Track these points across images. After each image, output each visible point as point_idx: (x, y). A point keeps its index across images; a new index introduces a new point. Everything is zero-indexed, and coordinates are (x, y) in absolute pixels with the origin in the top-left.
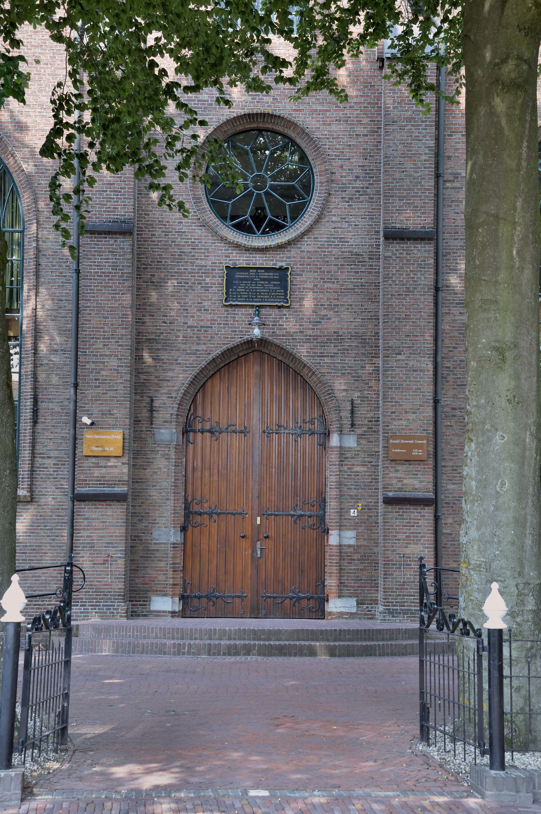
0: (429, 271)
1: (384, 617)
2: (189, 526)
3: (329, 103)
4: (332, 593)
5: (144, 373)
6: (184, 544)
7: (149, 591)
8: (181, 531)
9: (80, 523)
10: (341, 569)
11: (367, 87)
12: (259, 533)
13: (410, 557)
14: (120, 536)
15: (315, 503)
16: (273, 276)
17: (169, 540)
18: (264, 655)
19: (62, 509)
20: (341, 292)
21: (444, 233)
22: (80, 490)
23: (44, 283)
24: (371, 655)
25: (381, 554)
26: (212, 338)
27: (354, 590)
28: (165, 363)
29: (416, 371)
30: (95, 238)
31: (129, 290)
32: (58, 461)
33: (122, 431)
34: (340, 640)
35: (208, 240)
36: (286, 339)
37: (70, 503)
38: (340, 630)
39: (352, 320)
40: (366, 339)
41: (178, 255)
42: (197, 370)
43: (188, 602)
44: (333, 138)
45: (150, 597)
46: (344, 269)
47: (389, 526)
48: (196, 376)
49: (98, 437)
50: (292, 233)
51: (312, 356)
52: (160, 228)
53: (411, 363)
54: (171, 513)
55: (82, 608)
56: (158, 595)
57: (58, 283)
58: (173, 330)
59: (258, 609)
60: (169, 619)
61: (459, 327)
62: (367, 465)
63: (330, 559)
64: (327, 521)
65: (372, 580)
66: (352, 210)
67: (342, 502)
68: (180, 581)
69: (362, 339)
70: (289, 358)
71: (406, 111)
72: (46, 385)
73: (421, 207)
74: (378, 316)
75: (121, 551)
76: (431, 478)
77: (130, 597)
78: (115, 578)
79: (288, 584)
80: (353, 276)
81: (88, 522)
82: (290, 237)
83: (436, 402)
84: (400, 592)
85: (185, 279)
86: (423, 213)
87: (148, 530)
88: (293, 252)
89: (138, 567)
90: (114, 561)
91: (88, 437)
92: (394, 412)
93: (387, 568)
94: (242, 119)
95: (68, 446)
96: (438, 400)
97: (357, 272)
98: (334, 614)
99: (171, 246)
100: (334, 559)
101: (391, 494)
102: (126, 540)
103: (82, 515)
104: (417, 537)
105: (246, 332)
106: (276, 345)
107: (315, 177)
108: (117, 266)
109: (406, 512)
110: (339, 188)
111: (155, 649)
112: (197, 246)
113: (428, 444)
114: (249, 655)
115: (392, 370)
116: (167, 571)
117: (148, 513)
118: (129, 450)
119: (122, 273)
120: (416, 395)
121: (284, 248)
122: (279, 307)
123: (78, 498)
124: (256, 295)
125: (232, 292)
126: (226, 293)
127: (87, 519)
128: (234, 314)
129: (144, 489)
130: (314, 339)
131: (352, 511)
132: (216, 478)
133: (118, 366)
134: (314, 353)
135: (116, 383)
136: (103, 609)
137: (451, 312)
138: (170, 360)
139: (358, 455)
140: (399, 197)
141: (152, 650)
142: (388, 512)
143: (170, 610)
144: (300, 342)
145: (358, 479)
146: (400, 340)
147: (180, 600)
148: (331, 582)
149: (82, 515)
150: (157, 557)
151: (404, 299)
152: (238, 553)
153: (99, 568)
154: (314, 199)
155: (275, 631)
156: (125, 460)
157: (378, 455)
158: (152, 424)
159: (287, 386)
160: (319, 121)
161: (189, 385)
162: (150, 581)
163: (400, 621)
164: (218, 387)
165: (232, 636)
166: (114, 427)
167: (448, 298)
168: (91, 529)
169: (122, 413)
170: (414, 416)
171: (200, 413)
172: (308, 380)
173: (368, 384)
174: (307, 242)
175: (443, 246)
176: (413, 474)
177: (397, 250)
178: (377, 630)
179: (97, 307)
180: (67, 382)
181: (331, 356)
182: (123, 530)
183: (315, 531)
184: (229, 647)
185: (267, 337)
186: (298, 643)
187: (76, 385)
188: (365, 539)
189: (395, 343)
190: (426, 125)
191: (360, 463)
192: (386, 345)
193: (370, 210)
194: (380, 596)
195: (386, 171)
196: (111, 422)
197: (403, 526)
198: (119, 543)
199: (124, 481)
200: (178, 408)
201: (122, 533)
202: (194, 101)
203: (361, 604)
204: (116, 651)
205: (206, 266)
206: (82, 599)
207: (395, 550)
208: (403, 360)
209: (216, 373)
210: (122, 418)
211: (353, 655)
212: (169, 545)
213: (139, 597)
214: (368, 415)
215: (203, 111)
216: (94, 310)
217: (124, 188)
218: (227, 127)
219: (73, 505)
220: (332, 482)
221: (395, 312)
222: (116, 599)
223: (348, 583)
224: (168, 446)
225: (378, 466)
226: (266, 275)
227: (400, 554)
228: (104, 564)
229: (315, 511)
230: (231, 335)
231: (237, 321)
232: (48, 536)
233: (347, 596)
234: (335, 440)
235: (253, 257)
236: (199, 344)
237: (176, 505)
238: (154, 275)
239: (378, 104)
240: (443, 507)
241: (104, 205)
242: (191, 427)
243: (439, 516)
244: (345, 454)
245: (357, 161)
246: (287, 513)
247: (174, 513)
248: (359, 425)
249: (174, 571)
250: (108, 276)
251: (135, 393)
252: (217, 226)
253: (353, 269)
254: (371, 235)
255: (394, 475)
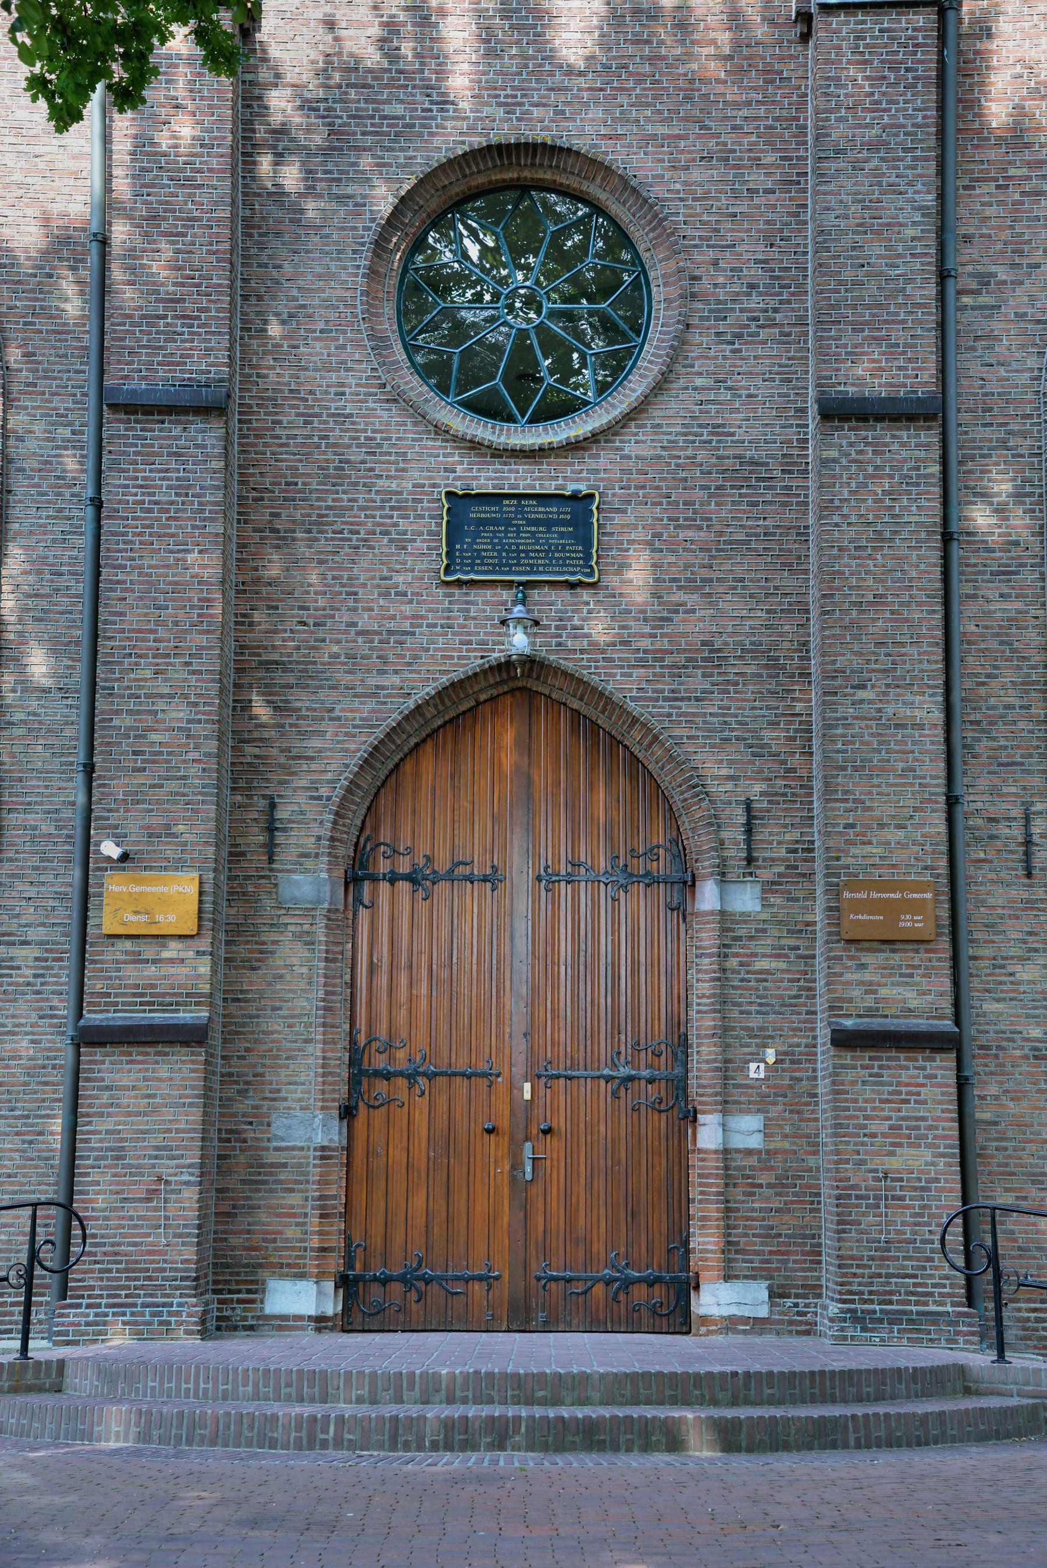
0: (927, 493)
1: (842, 1329)
2: (361, 1104)
3: (686, 119)
4: (709, 1268)
5: (255, 740)
6: (349, 1149)
7: (260, 1266)
8: (341, 1118)
9: (93, 1098)
10: (728, 1210)
11: (772, 81)
12: (528, 1121)
13: (901, 1180)
14: (188, 1131)
15: (663, 1047)
16: (558, 513)
17: (310, 1139)
18: (545, 1448)
19: (54, 1067)
20: (718, 550)
21: (959, 411)
22: (93, 1018)
23: (18, 533)
24: (834, 1446)
25: (828, 1171)
26: (415, 657)
27: (762, 1262)
28: (305, 718)
29: (903, 726)
30: (137, 421)
31: (216, 543)
32: (47, 951)
33: (196, 875)
34: (747, 1402)
35: (404, 432)
36: (589, 660)
37: (70, 1051)
38: (748, 1375)
39: (744, 613)
40: (777, 659)
41: (336, 468)
42: (380, 733)
43: (357, 1292)
44: (694, 199)
45: (264, 1282)
46: (723, 495)
47: (846, 1100)
48: (376, 748)
49: (137, 889)
50: (600, 416)
51: (651, 699)
52: (292, 407)
53: (890, 710)
54: (316, 1075)
55: (92, 1311)
56: (283, 1276)
57: (53, 532)
58: (324, 640)
59: (527, 1309)
60: (308, 1337)
61: (1001, 627)
62: (786, 956)
63: (701, 1185)
64: (692, 1091)
65: (805, 1236)
66: (739, 362)
67: (728, 1045)
68: (337, 1241)
69: (769, 658)
70: (597, 704)
71: (867, 126)
72: (20, 771)
73: (906, 345)
74: (807, 604)
75: (190, 1166)
76: (947, 984)
77: (215, 1282)
78: (175, 1236)
79: (599, 1247)
80: (744, 511)
81: (111, 1097)
82: (597, 425)
83: (952, 802)
84: (878, 1267)
85: (352, 524)
86: (910, 360)
87: (262, 1116)
88: (604, 459)
89: (234, 1207)
90: (173, 1191)
91: (115, 889)
92: (852, 826)
93: (846, 1206)
94: (484, 158)
95: (67, 914)
96: (957, 798)
97: (755, 504)
98: (714, 1322)
99: (318, 446)
100: (710, 1185)
101: (849, 1023)
102: (203, 1139)
103: (95, 1080)
104: (918, 1128)
105: (495, 643)
106: (565, 673)
107: (654, 290)
108: (189, 487)
109: (889, 1068)
110: (710, 311)
111: (246, 1433)
112: (380, 446)
113: (936, 901)
114: (502, 1448)
115: (846, 726)
116: (306, 1215)
117: (262, 1075)
118: (214, 921)
119: (200, 504)
120: (903, 785)
121: (584, 449)
122: (573, 586)
123: (90, 1038)
124: (518, 558)
125: (462, 551)
126: (448, 553)
127: (108, 1088)
128: (467, 603)
129: (251, 1017)
130: (655, 660)
131: (753, 1066)
132: (424, 990)
133: (189, 721)
134: (655, 691)
135: (185, 761)
136: (143, 1314)
137: (980, 593)
138: (315, 710)
139: (764, 931)
140: (852, 323)
141: (239, 1434)
142: (843, 1067)
143: (312, 1312)
144: (622, 667)
145: (765, 989)
146: (861, 654)
147: (336, 1287)
148: (705, 1242)
149: (95, 1080)
150: (281, 1182)
151: (870, 557)
152: (478, 1171)
153: (135, 1209)
154: (652, 340)
155: (574, 1377)
156: (204, 944)
157: (814, 932)
158: (271, 861)
159: (592, 769)
160: (663, 161)
161: (361, 767)
162: (265, 1240)
163: (882, 1340)
164: (430, 768)
165: (459, 1394)
166: (179, 865)
167: (973, 561)
168: (116, 1115)
169: (196, 830)
170: (901, 833)
171: (385, 835)
172: (640, 756)
173: (784, 762)
174: (636, 434)
175: (958, 441)
176: (901, 975)
177: (851, 444)
178: (842, 1372)
179: (140, 583)
180: (72, 763)
181: (697, 699)
182: (195, 1115)
183: (664, 1116)
184: (448, 1425)
185: (543, 654)
186: (635, 1412)
187: (89, 769)
188: (785, 1136)
189: (851, 661)
190: (915, 159)
191: (769, 951)
192: (829, 667)
193: (784, 361)
194: (828, 1275)
195: (820, 265)
196: (170, 854)
197: (882, 1101)
198: (186, 1148)
199: (201, 995)
200: (335, 822)
201: (194, 1122)
202: (373, 117)
203: (780, 1296)
204: (144, 1437)
205: (400, 493)
206: (92, 1288)
207: (863, 1162)
208: (871, 702)
209: (424, 741)
210: (198, 843)
211: (787, 1447)
212: (311, 1153)
213: (238, 1282)
214: (788, 837)
215: (394, 141)
216: (133, 591)
217: (207, 310)
218: (448, 176)
219: (78, 1054)
220: (703, 996)
221: (850, 588)
222: (177, 1288)
223: (746, 1244)
224: (309, 912)
225: (814, 957)
226: (540, 511)
227: (876, 1171)
228: (149, 1200)
229: (663, 1067)
230: (460, 650)
231: (474, 618)
232: (17, 1134)
233: (746, 1277)
234: (708, 897)
235: (510, 471)
236: (385, 672)
237: (329, 1054)
238: (278, 515)
239: (798, 119)
240: (974, 1056)
241: (160, 348)
242: (366, 868)
243: (967, 1079)
244: (733, 930)
245: (750, 249)
246: (597, 1073)
247: (324, 1075)
248: (765, 860)
249: (322, 1216)
250: (168, 511)
251: (233, 789)
252: (427, 401)
253: (746, 495)
254: (787, 418)
255: (856, 976)
